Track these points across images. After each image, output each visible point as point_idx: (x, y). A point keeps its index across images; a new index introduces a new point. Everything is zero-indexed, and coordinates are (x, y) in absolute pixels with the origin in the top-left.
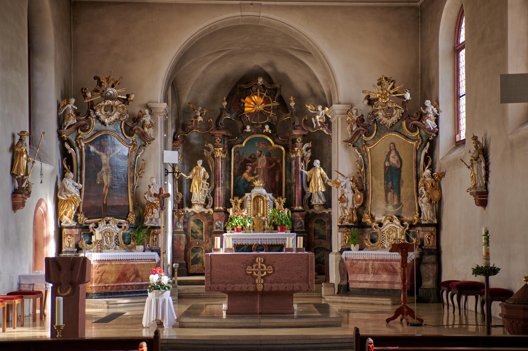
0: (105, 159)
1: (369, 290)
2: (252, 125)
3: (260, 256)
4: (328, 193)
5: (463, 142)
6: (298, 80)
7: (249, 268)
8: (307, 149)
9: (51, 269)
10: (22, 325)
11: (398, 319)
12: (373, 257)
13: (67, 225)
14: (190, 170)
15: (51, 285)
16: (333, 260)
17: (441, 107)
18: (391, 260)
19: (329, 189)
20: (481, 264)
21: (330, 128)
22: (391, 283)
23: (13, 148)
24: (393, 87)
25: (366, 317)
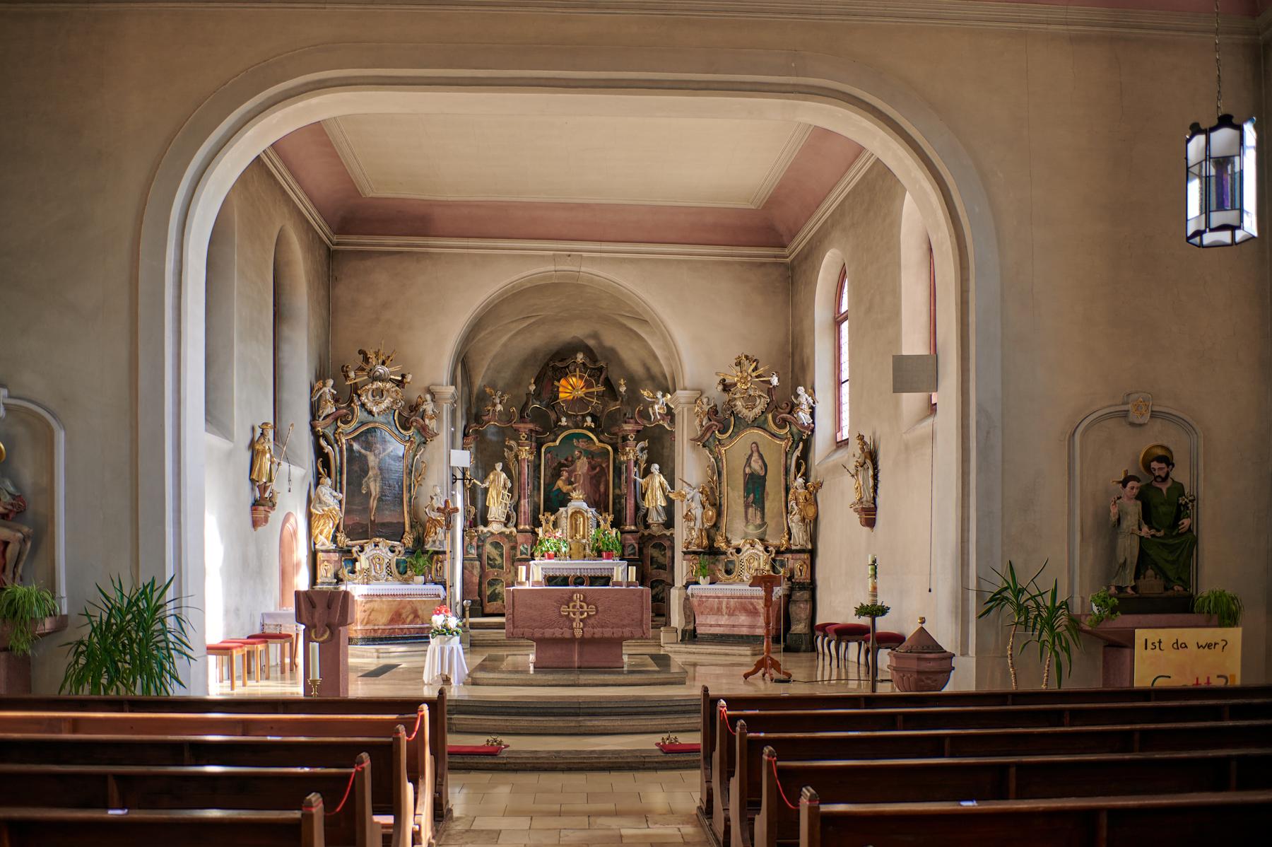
0: (372, 460)
1: (722, 636)
2: (568, 416)
3: (579, 591)
4: (669, 509)
5: (846, 442)
6: (631, 357)
7: (564, 608)
8: (642, 450)
9: (303, 606)
10: (267, 678)
11: (760, 673)
12: (729, 594)
13: (324, 548)
14: (486, 476)
15: (303, 627)
16: (675, 596)
17: (817, 396)
18: (752, 597)
19: (671, 503)
20: (867, 601)
21: (672, 421)
22: (752, 627)
23: (252, 445)
24: (755, 369)
25: (719, 670)
